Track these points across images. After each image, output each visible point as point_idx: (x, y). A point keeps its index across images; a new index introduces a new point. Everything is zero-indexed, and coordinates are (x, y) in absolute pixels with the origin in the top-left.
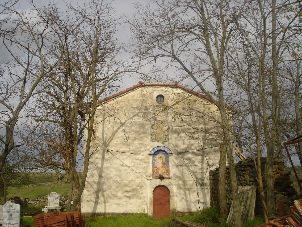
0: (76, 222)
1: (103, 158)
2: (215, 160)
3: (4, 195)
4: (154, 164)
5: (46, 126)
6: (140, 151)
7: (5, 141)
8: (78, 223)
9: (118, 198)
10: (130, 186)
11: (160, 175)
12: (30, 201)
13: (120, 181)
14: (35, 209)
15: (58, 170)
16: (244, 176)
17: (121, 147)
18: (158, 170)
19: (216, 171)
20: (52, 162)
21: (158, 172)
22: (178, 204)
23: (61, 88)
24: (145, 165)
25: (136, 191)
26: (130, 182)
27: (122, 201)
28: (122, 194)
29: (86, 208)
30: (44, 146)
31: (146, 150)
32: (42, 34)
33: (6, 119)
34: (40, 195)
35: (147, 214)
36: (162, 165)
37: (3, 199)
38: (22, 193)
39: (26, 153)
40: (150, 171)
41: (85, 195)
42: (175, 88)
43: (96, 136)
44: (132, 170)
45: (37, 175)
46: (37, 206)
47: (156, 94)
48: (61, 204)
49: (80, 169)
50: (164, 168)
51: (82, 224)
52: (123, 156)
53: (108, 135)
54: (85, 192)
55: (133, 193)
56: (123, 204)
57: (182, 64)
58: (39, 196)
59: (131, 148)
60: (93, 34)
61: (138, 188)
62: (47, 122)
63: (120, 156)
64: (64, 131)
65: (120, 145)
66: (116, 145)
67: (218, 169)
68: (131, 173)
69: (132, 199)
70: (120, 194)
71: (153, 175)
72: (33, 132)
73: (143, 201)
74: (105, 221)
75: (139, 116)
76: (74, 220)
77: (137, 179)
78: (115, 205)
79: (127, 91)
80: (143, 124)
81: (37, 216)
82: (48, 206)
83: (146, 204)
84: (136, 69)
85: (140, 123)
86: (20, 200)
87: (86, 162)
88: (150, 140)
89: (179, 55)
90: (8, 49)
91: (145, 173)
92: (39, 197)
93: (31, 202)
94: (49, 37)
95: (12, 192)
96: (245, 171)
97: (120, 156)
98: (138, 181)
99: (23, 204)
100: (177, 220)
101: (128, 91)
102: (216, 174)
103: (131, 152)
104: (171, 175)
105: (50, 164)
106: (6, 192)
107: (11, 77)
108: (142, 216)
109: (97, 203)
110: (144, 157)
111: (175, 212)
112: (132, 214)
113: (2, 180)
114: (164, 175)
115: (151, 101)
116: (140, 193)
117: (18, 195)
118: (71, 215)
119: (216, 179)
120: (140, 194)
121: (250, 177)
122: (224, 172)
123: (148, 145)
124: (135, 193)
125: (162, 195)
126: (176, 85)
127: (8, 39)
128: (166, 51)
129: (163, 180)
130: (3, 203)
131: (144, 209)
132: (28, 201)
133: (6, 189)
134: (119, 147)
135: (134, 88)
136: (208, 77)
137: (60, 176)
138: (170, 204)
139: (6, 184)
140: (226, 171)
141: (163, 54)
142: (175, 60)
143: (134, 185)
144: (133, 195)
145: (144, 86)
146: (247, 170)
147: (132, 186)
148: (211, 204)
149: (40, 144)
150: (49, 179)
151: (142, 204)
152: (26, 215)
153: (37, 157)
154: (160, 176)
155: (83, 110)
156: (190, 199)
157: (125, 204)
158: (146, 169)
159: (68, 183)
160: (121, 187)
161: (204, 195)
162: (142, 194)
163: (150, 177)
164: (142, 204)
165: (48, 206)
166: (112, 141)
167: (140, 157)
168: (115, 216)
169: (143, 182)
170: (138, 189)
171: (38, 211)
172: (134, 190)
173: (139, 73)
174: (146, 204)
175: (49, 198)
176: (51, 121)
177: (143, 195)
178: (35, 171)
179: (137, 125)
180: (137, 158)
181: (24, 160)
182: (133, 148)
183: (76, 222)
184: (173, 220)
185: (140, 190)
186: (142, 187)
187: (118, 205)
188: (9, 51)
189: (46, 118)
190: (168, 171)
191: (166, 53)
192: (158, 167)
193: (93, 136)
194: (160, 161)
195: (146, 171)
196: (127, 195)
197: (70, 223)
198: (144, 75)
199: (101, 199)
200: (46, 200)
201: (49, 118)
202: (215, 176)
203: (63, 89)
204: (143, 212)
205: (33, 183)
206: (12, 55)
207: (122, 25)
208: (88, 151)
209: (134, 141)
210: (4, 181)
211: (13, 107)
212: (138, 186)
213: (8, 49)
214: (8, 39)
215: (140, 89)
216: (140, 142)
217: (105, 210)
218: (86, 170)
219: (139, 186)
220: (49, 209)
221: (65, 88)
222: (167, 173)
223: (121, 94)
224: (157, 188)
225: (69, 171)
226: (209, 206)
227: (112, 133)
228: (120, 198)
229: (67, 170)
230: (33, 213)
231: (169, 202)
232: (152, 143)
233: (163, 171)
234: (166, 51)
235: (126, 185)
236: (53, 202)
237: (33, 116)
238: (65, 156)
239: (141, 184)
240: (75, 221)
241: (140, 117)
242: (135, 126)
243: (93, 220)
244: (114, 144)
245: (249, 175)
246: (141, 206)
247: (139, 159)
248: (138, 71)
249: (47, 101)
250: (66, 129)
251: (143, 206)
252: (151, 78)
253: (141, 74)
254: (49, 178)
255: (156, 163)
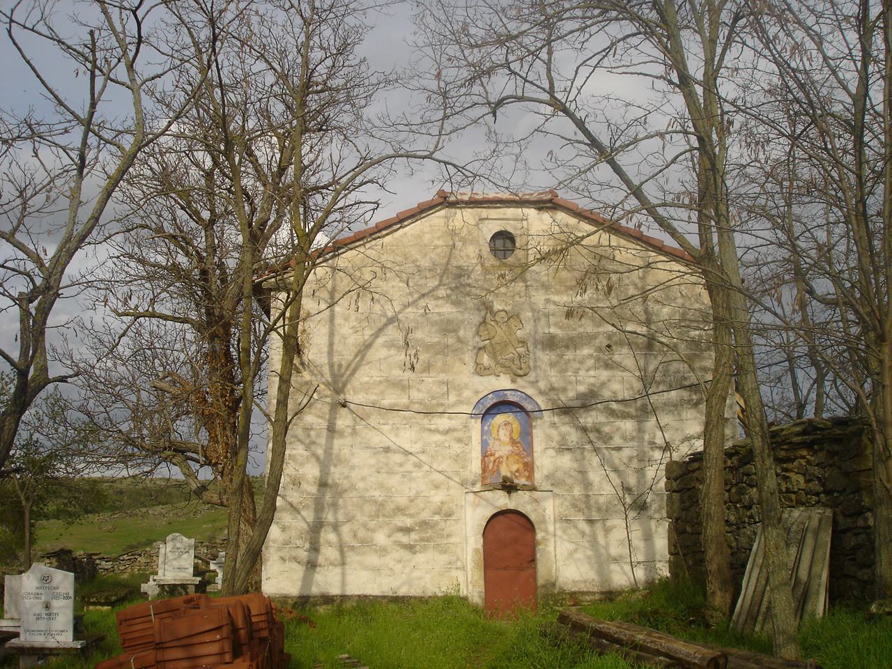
0: (259, 630)
1: (331, 430)
2: (685, 432)
3: (24, 544)
4: (484, 444)
5: (151, 333)
6: (443, 405)
7: (16, 360)
8: (265, 634)
9: (376, 551)
10: (412, 511)
11: (505, 479)
12: (104, 563)
13: (381, 499)
14: (120, 584)
15: (189, 468)
16: (788, 477)
17: (382, 393)
18: (498, 462)
19: (688, 463)
20: (170, 442)
21: (498, 471)
22: (566, 562)
23: (195, 215)
24: (457, 448)
25: (432, 527)
26: (412, 501)
27: (389, 560)
28: (389, 536)
29: (279, 579)
30: (144, 394)
31: (460, 402)
32: (137, 8)
33: (19, 286)
34: (134, 543)
35: (465, 599)
36: (509, 448)
37: (22, 555)
38: (81, 536)
39: (88, 414)
40: (475, 466)
41: (275, 541)
42: (548, 208)
43: (305, 358)
44: (418, 466)
45: (123, 486)
46: (125, 576)
47: (492, 228)
48: (197, 572)
49: (258, 462)
50: (517, 457)
51: (276, 633)
52: (391, 422)
53: (345, 353)
54: (274, 532)
55: (423, 533)
56: (391, 569)
57: (580, 124)
58: (132, 547)
59: (415, 395)
60: (291, 44)
61: (437, 518)
62: (154, 320)
63: (382, 422)
64: (206, 345)
65: (382, 387)
66: (366, 388)
67: (697, 458)
68: (414, 474)
69: (421, 552)
70: (381, 538)
71: (484, 478)
72: (111, 351)
73: (455, 558)
74: (340, 623)
75: (438, 298)
76: (252, 624)
77: (433, 492)
78: (371, 571)
79: (401, 221)
80: (449, 321)
81: (128, 607)
82: (160, 576)
83: (464, 568)
84: (432, 150)
85: (441, 320)
86: (74, 559)
87: (278, 439)
88: (473, 371)
89: (579, 91)
90: (23, 56)
91: (457, 473)
92: (132, 550)
93: (108, 565)
94: (161, 35)
95: (51, 533)
96: (793, 461)
97: (382, 422)
98: (437, 497)
99: (85, 572)
100: (574, 618)
101: (402, 220)
102: (689, 471)
103: (416, 407)
104: (538, 476)
105: (165, 449)
106: (31, 534)
107: (37, 156)
108: (451, 602)
109: (312, 565)
110: (456, 422)
111: (556, 596)
112: (421, 600)
113: (19, 497)
114: (516, 477)
115: (473, 254)
116: (444, 532)
117: (69, 545)
118: (243, 607)
119: (689, 490)
120: (442, 536)
121: (807, 481)
122: (720, 464)
123: (466, 386)
124: (429, 533)
125: (510, 540)
126: (550, 201)
127: (25, 27)
128: (532, 83)
129: (514, 495)
130: (22, 569)
131: (455, 583)
132: (98, 562)
133: (32, 525)
134: (376, 394)
135: (422, 212)
136: (677, 157)
137: (194, 486)
138: (535, 568)
139: (31, 512)
140: (725, 462)
141: (520, 94)
142: (560, 113)
143: (424, 510)
144: (422, 540)
145: (453, 205)
146: (796, 458)
147: (418, 514)
148: (673, 566)
149: (132, 386)
150: (161, 495)
151: (453, 567)
152: (94, 604)
153: (125, 427)
154: (504, 481)
155: (265, 280)
156: (600, 550)
157: (398, 567)
158: (460, 459)
159: (222, 504)
160: (384, 516)
161: (648, 538)
162: (449, 536)
163: (474, 484)
164: (453, 567)
165: (160, 576)
166: (356, 375)
167: (443, 422)
168: (366, 606)
169: (453, 501)
170: (437, 523)
171: (131, 592)
172: (424, 524)
173: (440, 161)
174: (464, 568)
175: (162, 551)
176: (166, 318)
177: (453, 540)
178: (120, 472)
179: (433, 324)
180: (433, 427)
181: (86, 439)
182: (421, 396)
183: (259, 630)
184: (563, 619)
185: (442, 524)
186: (450, 515)
187: (377, 570)
188: (28, 62)
189: (150, 309)
190: (529, 467)
191: (531, 91)
192: (497, 455)
193: (296, 361)
194: (504, 435)
195: (462, 468)
196: (405, 539)
197: (242, 632)
198: (454, 166)
199: (329, 553)
200: (152, 557)
201: (159, 308)
202: (685, 477)
203: (200, 219)
204: (453, 593)
205: (114, 509)
206: (38, 76)
207: (385, 10)
208: (282, 403)
209: (424, 375)
210: (24, 503)
211: (45, 251)
212: (438, 512)
213: (23, 56)
214: (25, 27)
215: (443, 213)
216: (443, 377)
217: (343, 583)
218: (279, 463)
219: (439, 514)
220: (162, 586)
221: (206, 215)
222: (527, 474)
223: (380, 231)
224: (501, 517)
225: (223, 468)
226: (664, 571)
227: (354, 350)
228: (383, 551)
229: (216, 464)
230: (114, 598)
231: (533, 560)
232: (477, 379)
233: (515, 467)
234: (532, 83)
235: (400, 510)
236: (175, 563)
237: (109, 314)
238: (207, 420)
239: (445, 508)
240: (255, 627)
241: (440, 302)
242: (427, 329)
243: (303, 620)
244: (361, 384)
245: (804, 475)
246: (447, 574)
247: (441, 429)
248: (437, 155)
249: (152, 255)
250: (212, 337)
251: (455, 573)
252: (475, 176)
253: (446, 163)
254: (161, 490)
255: (491, 442)
